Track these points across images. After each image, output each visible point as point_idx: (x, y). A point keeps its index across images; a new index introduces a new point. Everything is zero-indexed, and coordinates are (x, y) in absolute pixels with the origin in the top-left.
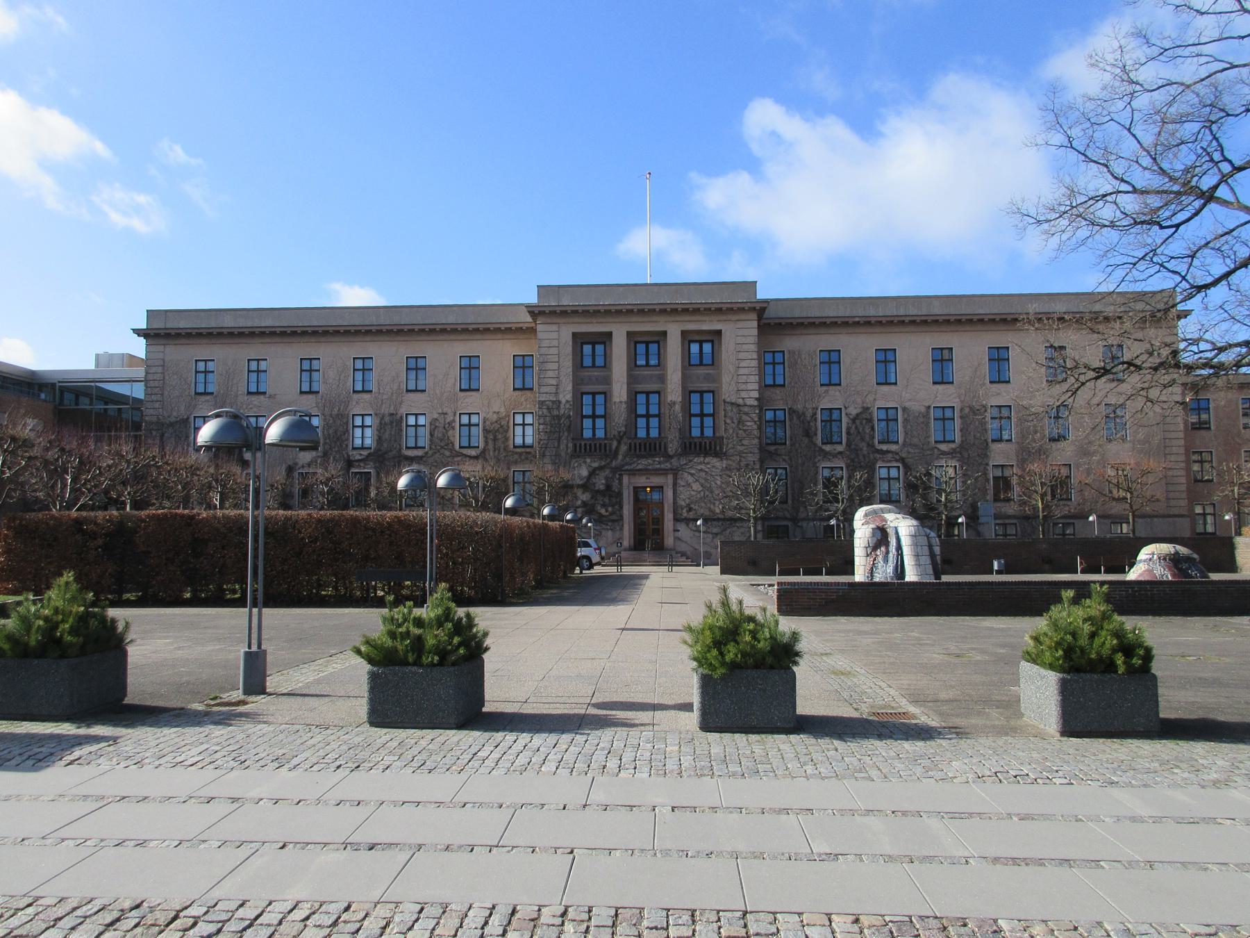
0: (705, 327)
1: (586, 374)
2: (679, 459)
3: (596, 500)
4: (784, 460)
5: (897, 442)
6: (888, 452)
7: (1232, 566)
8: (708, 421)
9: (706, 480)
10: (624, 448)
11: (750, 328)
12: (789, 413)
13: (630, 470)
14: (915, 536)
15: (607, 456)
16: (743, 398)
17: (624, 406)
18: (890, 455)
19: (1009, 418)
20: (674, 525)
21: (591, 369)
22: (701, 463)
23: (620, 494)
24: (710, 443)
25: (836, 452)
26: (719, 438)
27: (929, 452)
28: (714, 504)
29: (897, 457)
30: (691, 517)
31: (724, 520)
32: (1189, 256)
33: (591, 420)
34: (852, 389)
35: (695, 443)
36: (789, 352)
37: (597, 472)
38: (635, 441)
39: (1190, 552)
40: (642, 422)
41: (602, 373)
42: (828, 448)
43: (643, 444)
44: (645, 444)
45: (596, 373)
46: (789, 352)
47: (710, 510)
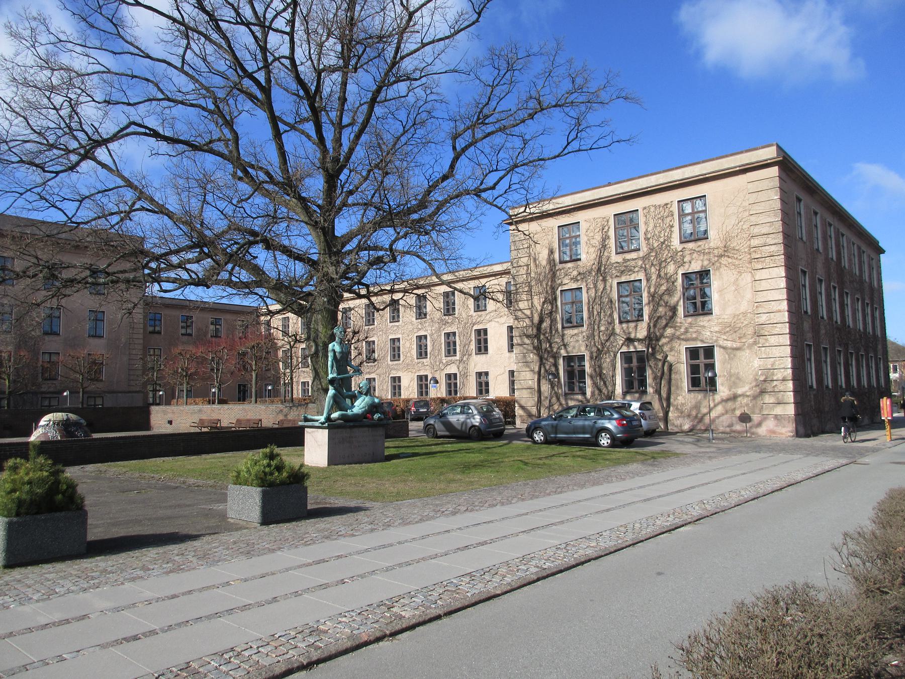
7: (148, 427)
19: (59, 317)
32: (78, 201)
39: (79, 418)
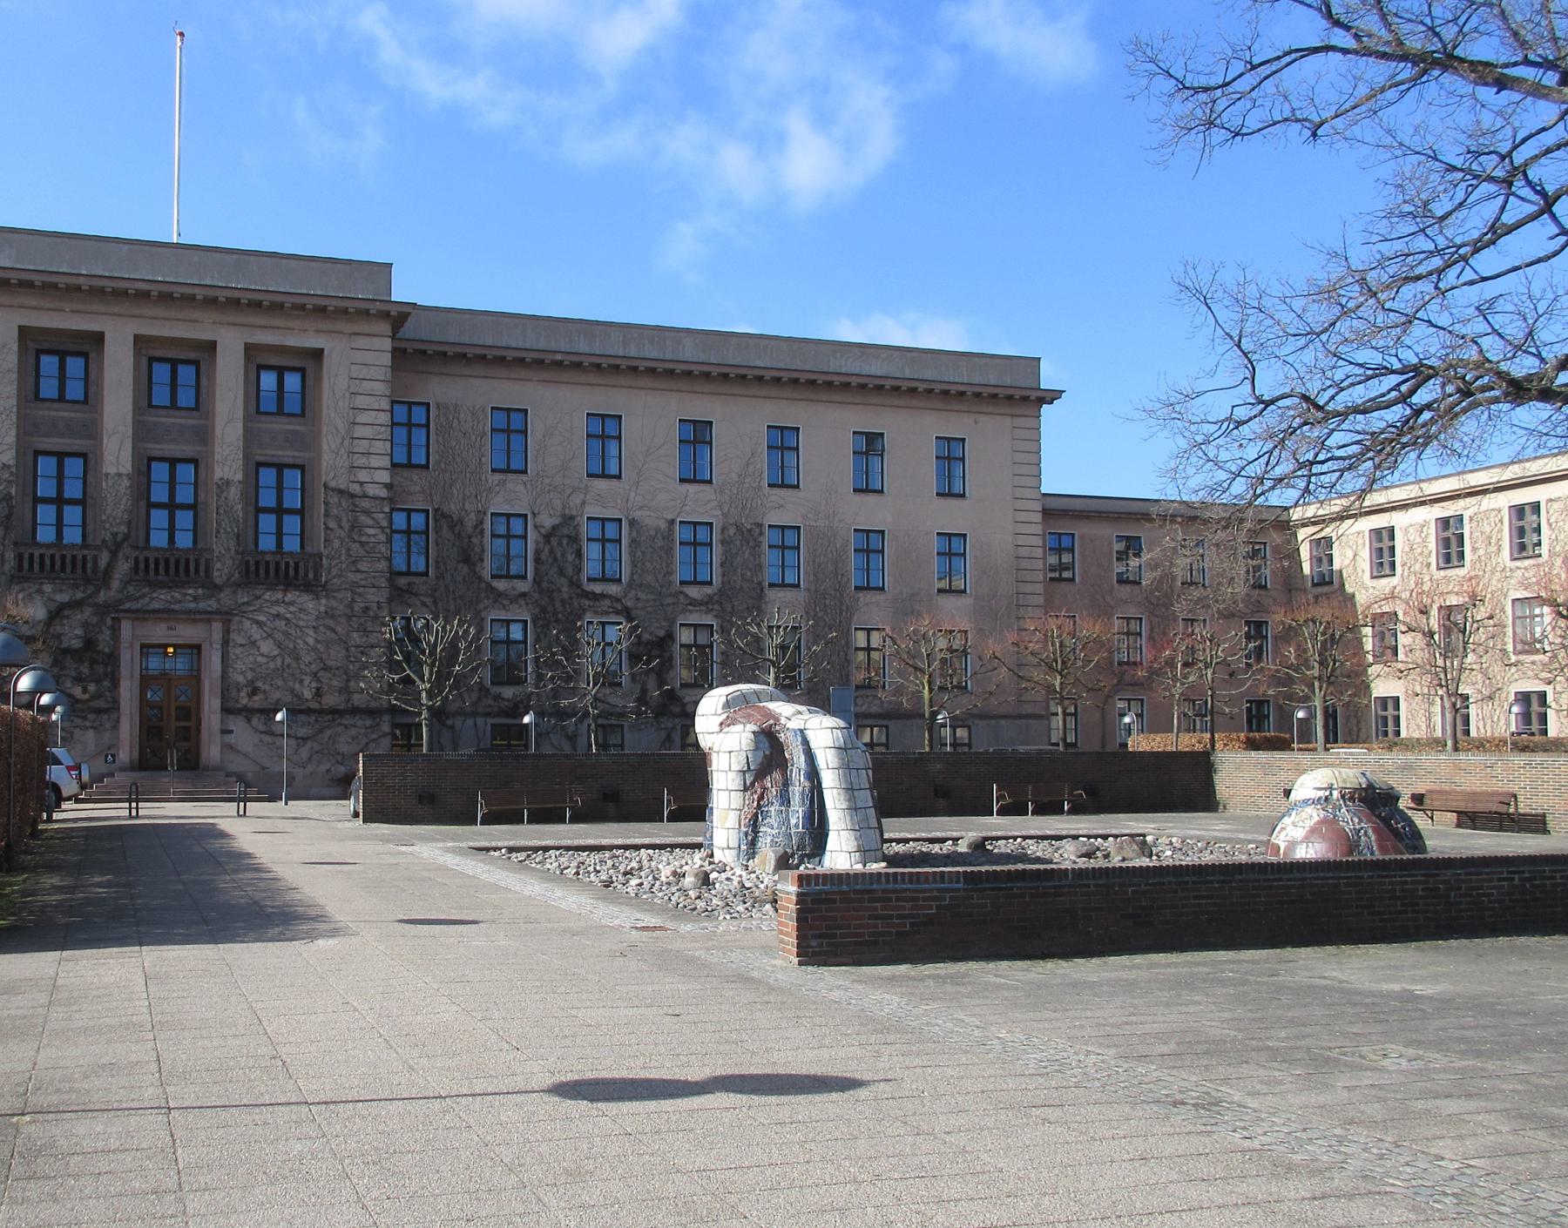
0: (292, 341)
1: (44, 413)
2: (235, 592)
3: (63, 668)
4: (424, 604)
5: (619, 580)
6: (603, 596)
8: (292, 524)
9: (286, 634)
10: (123, 567)
11: (376, 351)
12: (436, 520)
13: (137, 611)
14: (845, 749)
15: (88, 581)
16: (362, 483)
17: (126, 483)
18: (607, 602)
20: (222, 721)
21: (56, 405)
22: (277, 602)
23: (113, 658)
24: (296, 564)
25: (516, 593)
26: (311, 555)
27: (670, 600)
28: (301, 681)
29: (619, 607)
30: (256, 706)
31: (321, 712)
33: (67, 495)
34: (547, 481)
35: (267, 563)
36: (438, 406)
37: (66, 613)
38: (147, 553)
40: (159, 518)
41: (78, 415)
42: (501, 585)
43: (162, 562)
44: (167, 561)
45: (66, 414)
46: (438, 406)
47: (292, 691)
